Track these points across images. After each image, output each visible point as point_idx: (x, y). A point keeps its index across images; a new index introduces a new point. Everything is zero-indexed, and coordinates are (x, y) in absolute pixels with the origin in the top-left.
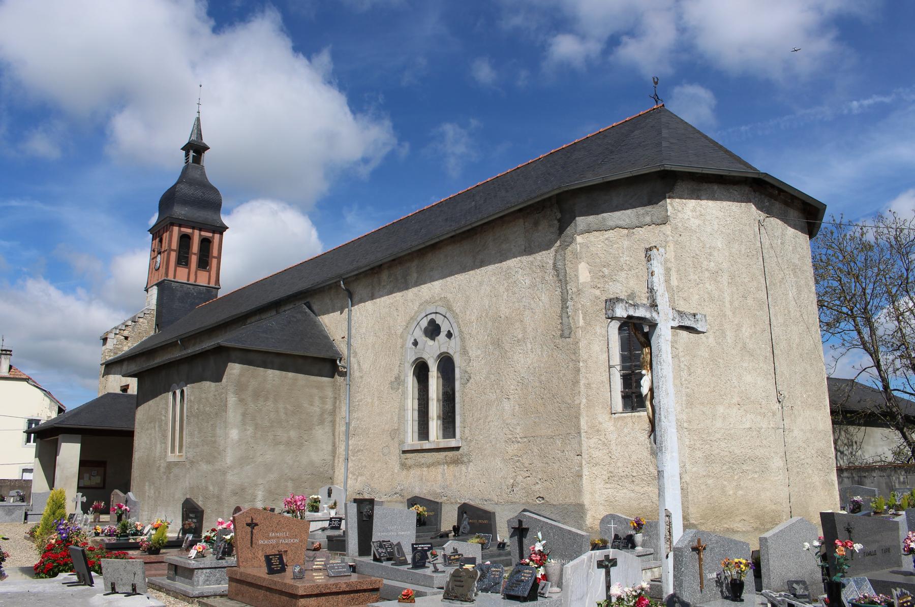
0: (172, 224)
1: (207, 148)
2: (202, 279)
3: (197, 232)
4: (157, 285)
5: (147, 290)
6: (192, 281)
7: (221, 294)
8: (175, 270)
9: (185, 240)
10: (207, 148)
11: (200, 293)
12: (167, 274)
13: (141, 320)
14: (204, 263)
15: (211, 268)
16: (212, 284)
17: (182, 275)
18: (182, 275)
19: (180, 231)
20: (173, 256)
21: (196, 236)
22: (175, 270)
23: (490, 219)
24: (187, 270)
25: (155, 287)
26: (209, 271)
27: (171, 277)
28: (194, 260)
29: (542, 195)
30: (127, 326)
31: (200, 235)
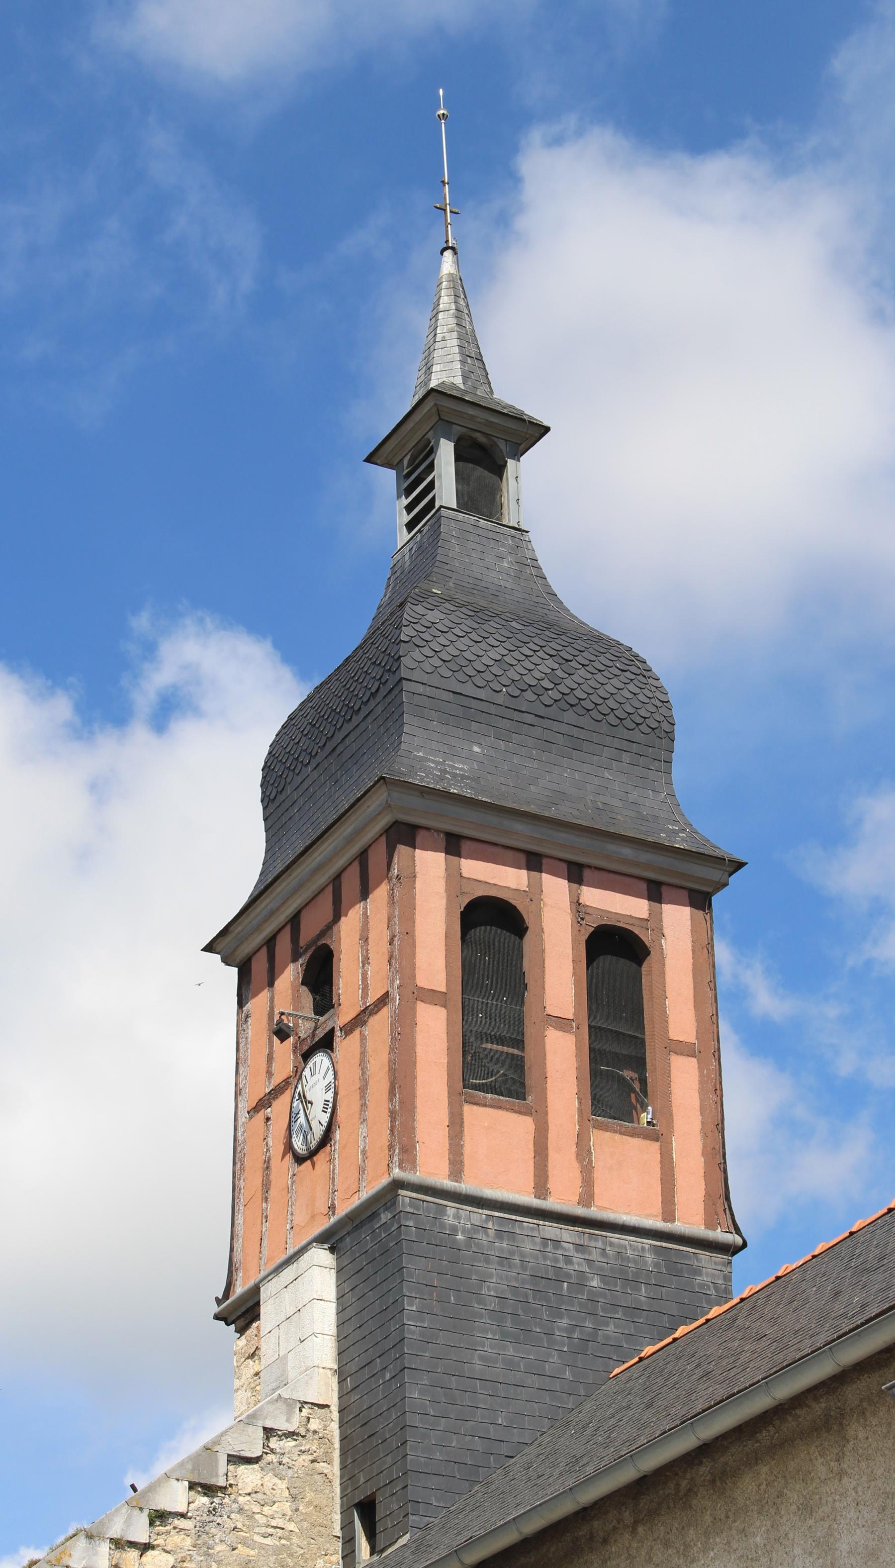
0: (404, 834)
1: (528, 432)
2: (627, 1181)
3: (555, 888)
4: (330, 1239)
5: (242, 1313)
6: (563, 1197)
7: (748, 1276)
8: (456, 1126)
9: (490, 925)
10: (528, 432)
11: (623, 1275)
12: (403, 1143)
13: (248, 1477)
14: (620, 1079)
15: (666, 1112)
16: (690, 1220)
17: (496, 1153)
18: (496, 1153)
19: (454, 878)
20: (435, 1034)
21: (558, 913)
22: (456, 1126)
23: (784, 1391)
24: (524, 1125)
25: (322, 1256)
26: (657, 1134)
27: (431, 1168)
28: (561, 1060)
29: (690, 1421)
30: (159, 1517)
31: (579, 909)
